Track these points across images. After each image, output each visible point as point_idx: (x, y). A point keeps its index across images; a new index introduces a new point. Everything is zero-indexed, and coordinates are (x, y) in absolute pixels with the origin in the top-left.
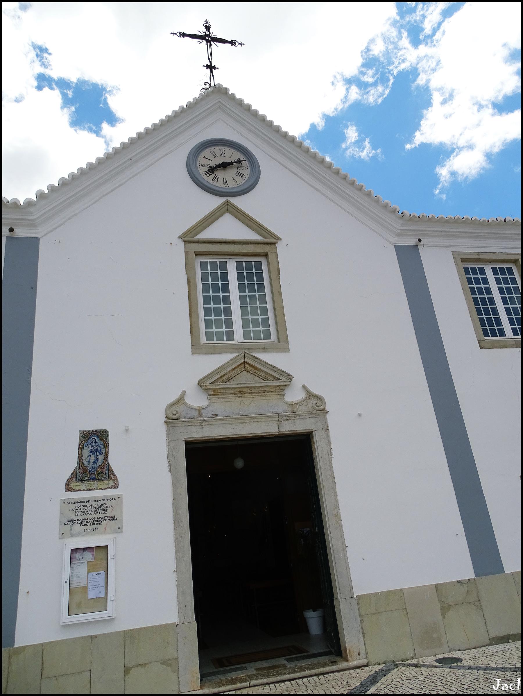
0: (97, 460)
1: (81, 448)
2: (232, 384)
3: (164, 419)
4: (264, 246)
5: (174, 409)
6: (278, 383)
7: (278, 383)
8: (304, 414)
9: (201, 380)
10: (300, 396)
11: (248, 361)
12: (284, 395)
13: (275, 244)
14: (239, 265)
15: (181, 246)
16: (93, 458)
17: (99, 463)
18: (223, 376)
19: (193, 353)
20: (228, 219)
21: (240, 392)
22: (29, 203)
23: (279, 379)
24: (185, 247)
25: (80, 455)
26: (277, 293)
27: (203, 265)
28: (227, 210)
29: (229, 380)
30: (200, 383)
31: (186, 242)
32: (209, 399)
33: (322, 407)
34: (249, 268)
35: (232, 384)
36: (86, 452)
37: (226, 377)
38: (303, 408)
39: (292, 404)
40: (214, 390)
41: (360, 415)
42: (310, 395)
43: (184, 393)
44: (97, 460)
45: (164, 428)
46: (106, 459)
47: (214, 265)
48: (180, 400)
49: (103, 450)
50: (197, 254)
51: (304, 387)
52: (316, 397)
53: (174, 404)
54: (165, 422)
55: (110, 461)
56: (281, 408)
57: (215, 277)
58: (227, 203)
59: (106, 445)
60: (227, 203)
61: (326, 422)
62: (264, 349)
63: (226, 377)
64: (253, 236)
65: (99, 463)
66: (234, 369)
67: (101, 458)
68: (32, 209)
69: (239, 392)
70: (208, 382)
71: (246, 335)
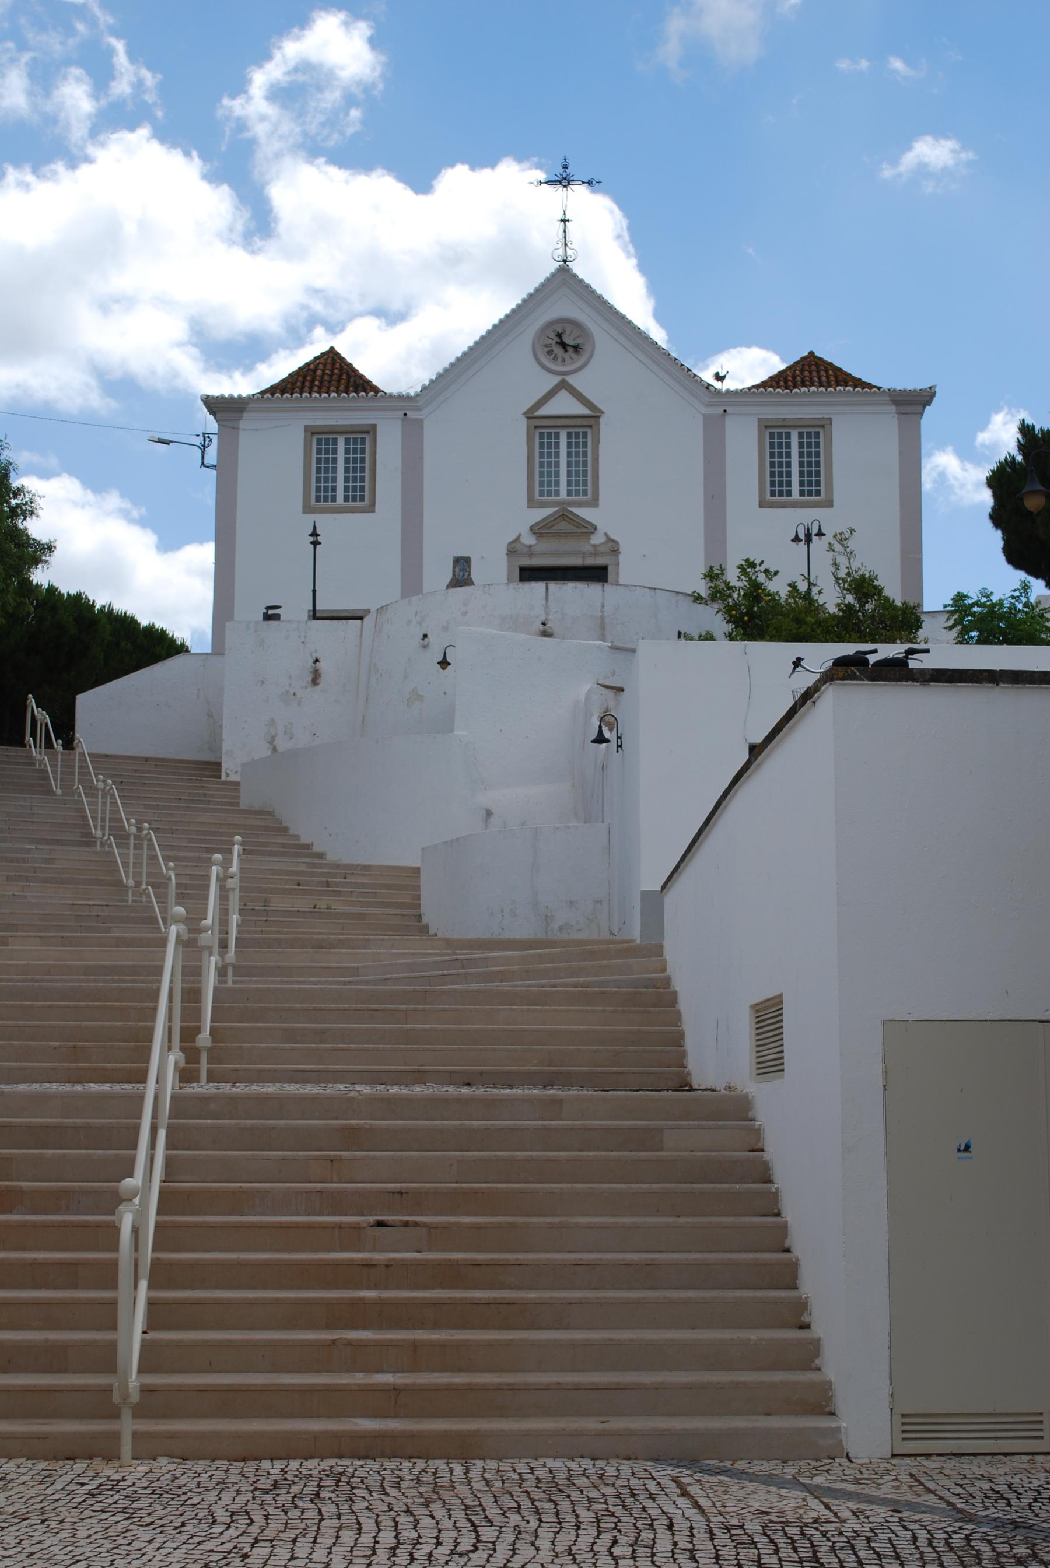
0: (464, 575)
1: (454, 567)
2: (553, 530)
3: (506, 552)
4: (589, 419)
5: (513, 545)
6: (585, 530)
7: (585, 530)
8: (602, 553)
9: (533, 525)
10: (603, 539)
11: (566, 513)
12: (590, 539)
13: (599, 417)
14: (801, 435)
15: (524, 421)
16: (462, 573)
17: (466, 577)
18: (547, 524)
19: (318, 615)
20: (564, 395)
21: (559, 536)
22: (417, 395)
23: (586, 527)
24: (528, 423)
25: (454, 571)
26: (596, 460)
27: (541, 436)
28: (563, 387)
29: (552, 526)
30: (531, 528)
31: (529, 418)
32: (537, 539)
33: (616, 549)
34: (327, 443)
35: (553, 530)
36: (457, 570)
37: (550, 524)
38: (602, 549)
39: (595, 546)
40: (541, 533)
41: (644, 556)
42: (610, 540)
43: (520, 535)
44: (464, 575)
45: (506, 557)
46: (470, 575)
47: (355, 441)
48: (517, 540)
49: (468, 570)
50: (536, 427)
51: (606, 534)
52: (613, 541)
53: (513, 542)
54: (507, 554)
55: (472, 576)
56: (587, 548)
57: (326, 470)
58: (563, 381)
59: (469, 566)
60: (563, 381)
61: (618, 559)
62: (580, 505)
63: (550, 524)
64: (586, 412)
65: (466, 577)
66: (555, 519)
67: (467, 574)
68: (418, 399)
69: (558, 535)
70: (536, 528)
71: (569, 493)
